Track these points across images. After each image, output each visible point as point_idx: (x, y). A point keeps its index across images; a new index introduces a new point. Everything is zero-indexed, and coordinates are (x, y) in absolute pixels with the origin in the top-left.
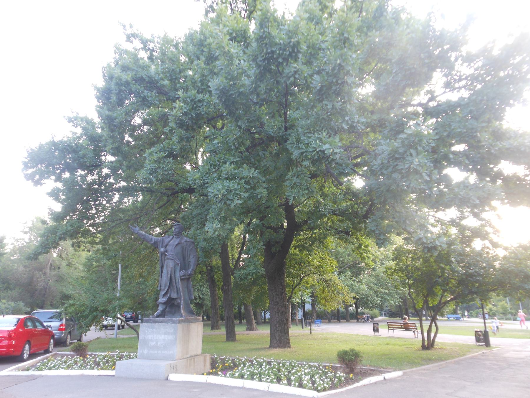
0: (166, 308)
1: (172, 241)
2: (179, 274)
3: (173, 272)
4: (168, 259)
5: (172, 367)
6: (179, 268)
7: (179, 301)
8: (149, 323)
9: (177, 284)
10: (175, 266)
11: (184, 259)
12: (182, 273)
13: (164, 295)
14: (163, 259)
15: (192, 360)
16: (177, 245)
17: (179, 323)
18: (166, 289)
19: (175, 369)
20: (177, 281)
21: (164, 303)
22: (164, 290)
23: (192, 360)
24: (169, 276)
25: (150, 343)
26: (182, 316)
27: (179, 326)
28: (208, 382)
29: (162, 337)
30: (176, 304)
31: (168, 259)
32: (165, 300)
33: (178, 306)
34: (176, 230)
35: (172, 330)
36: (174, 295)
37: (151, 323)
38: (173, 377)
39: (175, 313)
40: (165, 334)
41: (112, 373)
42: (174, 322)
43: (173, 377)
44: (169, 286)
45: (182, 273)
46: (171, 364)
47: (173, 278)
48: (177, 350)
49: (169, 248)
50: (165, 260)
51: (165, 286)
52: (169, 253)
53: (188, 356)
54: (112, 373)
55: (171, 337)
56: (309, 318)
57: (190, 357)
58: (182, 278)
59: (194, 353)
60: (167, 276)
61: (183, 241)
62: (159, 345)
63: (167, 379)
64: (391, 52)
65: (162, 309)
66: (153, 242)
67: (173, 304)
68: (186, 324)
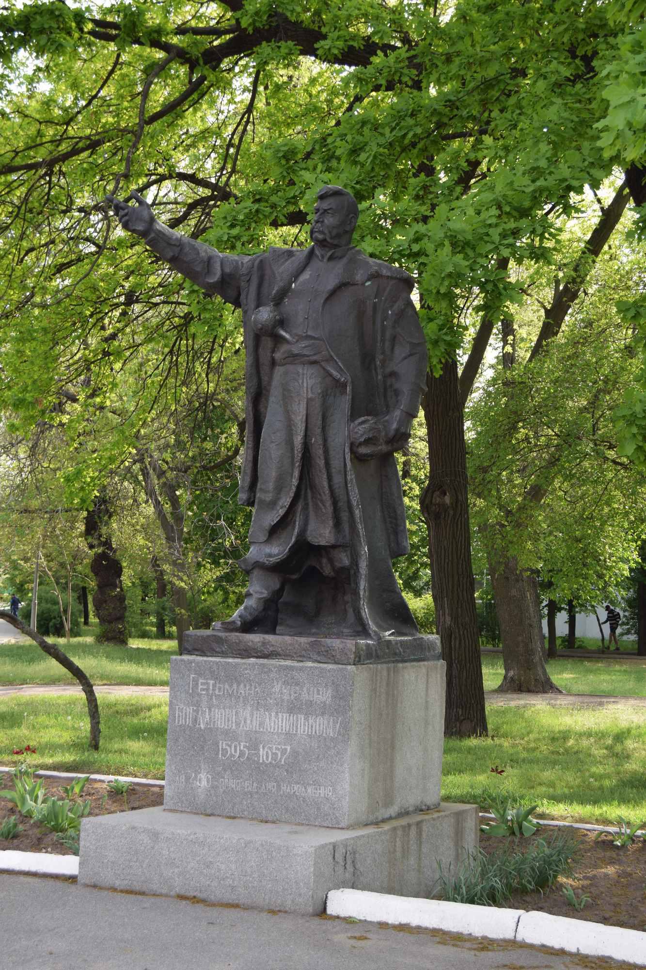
0: (281, 590)
1: (306, 276)
2: (343, 432)
3: (317, 421)
4: (293, 358)
5: (339, 857)
6: (344, 403)
7: (344, 559)
8: (214, 653)
9: (337, 479)
10: (325, 395)
11: (367, 359)
12: (362, 428)
13: (274, 531)
14: (265, 359)
15: (413, 831)
16: (333, 293)
17: (358, 660)
18: (286, 501)
19: (350, 868)
20: (336, 464)
21: (276, 569)
22: (273, 504)
23: (413, 831)
24: (298, 440)
25: (222, 745)
26: (362, 630)
27: (359, 676)
28: (519, 938)
29: (277, 723)
30: (327, 571)
31: (293, 358)
32: (276, 551)
33: (344, 580)
34: (329, 220)
35: (325, 696)
36: (322, 533)
37: (224, 654)
38: (347, 902)
39: (318, 613)
40: (293, 708)
41: (66, 864)
42: (329, 656)
43: (347, 902)
44: (299, 488)
45: (362, 428)
46: (335, 846)
47: (318, 452)
48: (345, 784)
49: (298, 308)
50: (273, 363)
51: (279, 489)
52: (300, 331)
53: (393, 811)
54: (66, 864)
55: (321, 725)
56: (388, 670)
57: (400, 815)
58: (363, 450)
59: (412, 799)
60: (290, 442)
61: (359, 277)
62: (264, 754)
63: (322, 912)
64: (304, 60)
65: (265, 594)
66: (214, 279)
67: (314, 573)
68: (382, 668)
